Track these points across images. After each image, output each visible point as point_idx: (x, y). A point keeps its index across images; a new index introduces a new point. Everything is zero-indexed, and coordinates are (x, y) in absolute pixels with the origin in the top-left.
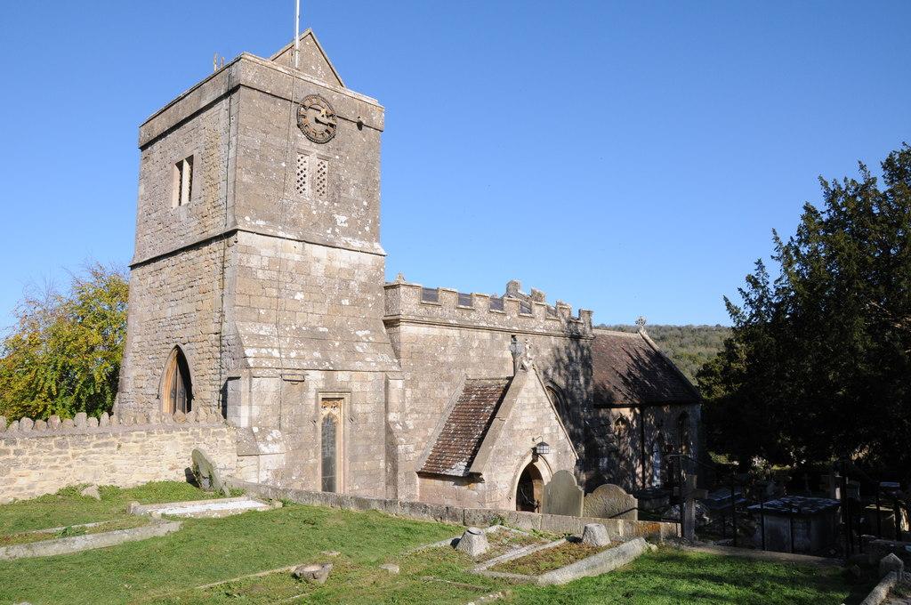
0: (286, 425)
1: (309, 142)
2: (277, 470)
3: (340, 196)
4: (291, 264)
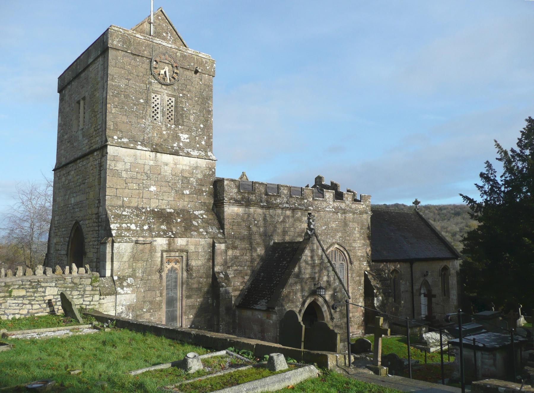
0: (139, 274)
1: (160, 86)
2: (130, 305)
3: (183, 122)
4: (147, 168)
